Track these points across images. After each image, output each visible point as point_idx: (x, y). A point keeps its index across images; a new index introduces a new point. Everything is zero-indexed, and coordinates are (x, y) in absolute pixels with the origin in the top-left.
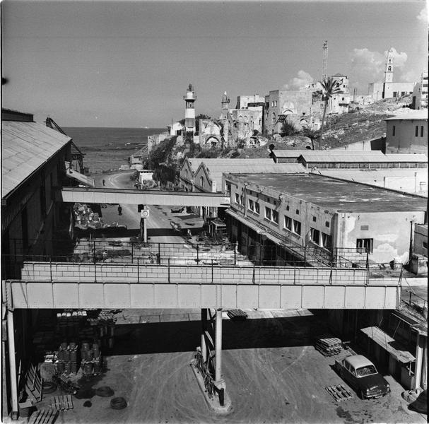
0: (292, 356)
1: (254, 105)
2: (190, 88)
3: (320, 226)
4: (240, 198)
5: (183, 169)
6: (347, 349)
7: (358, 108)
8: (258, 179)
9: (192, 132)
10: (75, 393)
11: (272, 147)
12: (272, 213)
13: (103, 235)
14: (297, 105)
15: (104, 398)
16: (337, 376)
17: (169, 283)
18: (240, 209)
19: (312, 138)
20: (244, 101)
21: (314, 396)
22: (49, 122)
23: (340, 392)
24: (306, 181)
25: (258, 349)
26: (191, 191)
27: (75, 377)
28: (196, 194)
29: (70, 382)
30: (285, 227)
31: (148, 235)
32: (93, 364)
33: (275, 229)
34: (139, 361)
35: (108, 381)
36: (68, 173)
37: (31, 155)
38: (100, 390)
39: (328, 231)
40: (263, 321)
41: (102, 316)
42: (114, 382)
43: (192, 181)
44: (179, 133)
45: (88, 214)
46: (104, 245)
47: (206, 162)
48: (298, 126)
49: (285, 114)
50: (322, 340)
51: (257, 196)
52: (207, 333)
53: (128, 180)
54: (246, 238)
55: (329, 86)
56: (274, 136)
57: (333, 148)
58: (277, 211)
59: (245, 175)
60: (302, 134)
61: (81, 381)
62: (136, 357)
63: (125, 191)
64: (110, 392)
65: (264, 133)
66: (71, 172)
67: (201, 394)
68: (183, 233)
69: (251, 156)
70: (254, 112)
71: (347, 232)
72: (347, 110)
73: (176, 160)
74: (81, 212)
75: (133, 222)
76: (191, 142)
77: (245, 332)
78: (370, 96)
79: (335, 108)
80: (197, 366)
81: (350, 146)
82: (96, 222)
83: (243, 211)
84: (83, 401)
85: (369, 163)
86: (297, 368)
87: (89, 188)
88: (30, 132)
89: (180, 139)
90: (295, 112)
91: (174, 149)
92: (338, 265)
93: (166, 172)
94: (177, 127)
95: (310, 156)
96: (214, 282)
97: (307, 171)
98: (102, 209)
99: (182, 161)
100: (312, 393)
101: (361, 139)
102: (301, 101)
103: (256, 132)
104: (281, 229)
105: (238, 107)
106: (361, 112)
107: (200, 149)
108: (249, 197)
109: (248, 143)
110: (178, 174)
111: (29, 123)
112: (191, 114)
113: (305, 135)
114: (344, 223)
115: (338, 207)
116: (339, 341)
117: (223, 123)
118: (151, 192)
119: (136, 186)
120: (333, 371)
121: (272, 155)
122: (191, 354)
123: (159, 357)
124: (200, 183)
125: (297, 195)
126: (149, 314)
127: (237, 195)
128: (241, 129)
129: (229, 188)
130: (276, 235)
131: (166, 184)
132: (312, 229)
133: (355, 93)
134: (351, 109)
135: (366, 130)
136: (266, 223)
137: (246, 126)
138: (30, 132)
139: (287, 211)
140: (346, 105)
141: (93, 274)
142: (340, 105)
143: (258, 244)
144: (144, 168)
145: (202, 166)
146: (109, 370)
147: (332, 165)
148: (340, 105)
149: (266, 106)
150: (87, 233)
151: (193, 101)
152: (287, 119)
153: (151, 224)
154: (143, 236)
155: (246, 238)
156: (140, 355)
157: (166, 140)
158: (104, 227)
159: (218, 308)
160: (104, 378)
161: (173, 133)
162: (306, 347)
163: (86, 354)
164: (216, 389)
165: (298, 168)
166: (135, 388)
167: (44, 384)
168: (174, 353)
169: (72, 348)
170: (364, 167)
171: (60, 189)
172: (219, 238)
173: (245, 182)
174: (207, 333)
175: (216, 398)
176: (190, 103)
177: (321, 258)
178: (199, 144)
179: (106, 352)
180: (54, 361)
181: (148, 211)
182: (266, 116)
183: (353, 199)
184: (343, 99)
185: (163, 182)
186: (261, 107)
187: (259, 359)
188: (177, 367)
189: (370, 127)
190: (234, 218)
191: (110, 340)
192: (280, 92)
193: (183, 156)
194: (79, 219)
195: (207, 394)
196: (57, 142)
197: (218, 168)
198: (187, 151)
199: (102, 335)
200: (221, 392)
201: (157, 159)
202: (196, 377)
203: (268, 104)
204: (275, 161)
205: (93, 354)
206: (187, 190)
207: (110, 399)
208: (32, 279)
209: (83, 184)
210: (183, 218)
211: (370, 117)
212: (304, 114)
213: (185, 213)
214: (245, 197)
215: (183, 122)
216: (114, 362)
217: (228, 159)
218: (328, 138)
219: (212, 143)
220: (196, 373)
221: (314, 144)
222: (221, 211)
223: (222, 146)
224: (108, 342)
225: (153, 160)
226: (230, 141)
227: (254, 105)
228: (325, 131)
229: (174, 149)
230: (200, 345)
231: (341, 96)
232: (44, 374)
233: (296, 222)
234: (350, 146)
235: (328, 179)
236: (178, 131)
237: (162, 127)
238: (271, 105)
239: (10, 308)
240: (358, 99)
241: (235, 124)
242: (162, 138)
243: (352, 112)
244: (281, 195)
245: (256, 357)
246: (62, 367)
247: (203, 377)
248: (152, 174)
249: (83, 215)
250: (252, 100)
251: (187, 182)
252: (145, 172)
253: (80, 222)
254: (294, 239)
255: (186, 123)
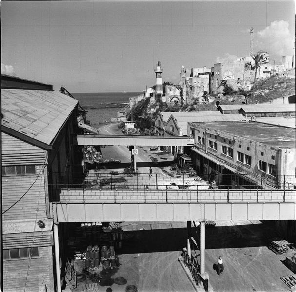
0: (252, 254)
1: (203, 74)
2: (159, 64)
3: (267, 159)
4: (201, 139)
5: (157, 120)
6: (292, 248)
7: (277, 74)
8: (214, 126)
9: (161, 94)
10: (99, 282)
11: (218, 103)
12: (227, 150)
13: (104, 167)
14: (235, 73)
15: (121, 285)
16: (288, 269)
17: (167, 203)
18: (201, 148)
19: (245, 95)
20: (196, 72)
21: (273, 284)
22: (63, 90)
23: (293, 281)
24: (248, 126)
25: (226, 249)
26: (163, 135)
27: (98, 270)
28: (167, 137)
29: (95, 274)
30: (238, 160)
31: (137, 167)
32: (110, 260)
33: (230, 161)
34: (174, 253)
35: (121, 273)
36: (79, 124)
37: (58, 113)
38: (117, 279)
39: (273, 162)
40: (227, 228)
41: (83, 225)
42: (126, 273)
43: (164, 128)
44: (151, 95)
45: (93, 153)
46: (106, 174)
47: (175, 114)
48: (235, 88)
49: (226, 79)
50: (275, 242)
51: (216, 138)
52: (192, 238)
53: (117, 128)
54: (207, 167)
55: (257, 59)
56: (219, 95)
57: (261, 102)
58: (232, 148)
59: (204, 123)
60: (239, 93)
61: (103, 273)
62: (139, 254)
63: (121, 136)
64: (124, 281)
65: (211, 92)
66: (81, 124)
67: (190, 283)
68: (162, 165)
69: (203, 110)
70: (204, 79)
71: (288, 163)
72: (269, 75)
73: (150, 114)
74: (89, 151)
75: (124, 158)
76: (160, 101)
77: (223, 237)
78: (283, 66)
79: (262, 76)
80: (185, 262)
81: (274, 101)
82: (100, 158)
83: (204, 149)
84: (106, 287)
85: (290, 112)
86: (258, 263)
87: (94, 135)
88: (52, 97)
89: (153, 99)
90: (233, 78)
91: (149, 106)
92: (282, 188)
93: (144, 123)
94: (150, 91)
95: (247, 108)
96: (199, 202)
97: (248, 119)
98: (101, 149)
99: (154, 114)
100: (271, 282)
101: (281, 95)
102: (237, 70)
103: (205, 93)
104: (235, 162)
105: (192, 75)
106: (280, 77)
107: (166, 106)
108: (209, 139)
109: (200, 100)
110: (153, 123)
111: (50, 91)
112: (159, 81)
113: (240, 94)
114: (286, 156)
115: (278, 145)
116: (287, 243)
117: (182, 87)
118: (133, 137)
119: (124, 132)
120: (284, 265)
121: (219, 109)
122: (178, 253)
123: (156, 254)
124: (170, 129)
125: (246, 136)
126: (145, 224)
127: (200, 138)
128: (196, 91)
129: (193, 134)
130: (231, 166)
131: (144, 131)
132: (260, 161)
133: (274, 64)
134: (272, 75)
135: (284, 89)
136: (222, 157)
137: (199, 89)
138: (52, 97)
139: (240, 149)
140: (268, 72)
141: (113, 197)
142: (264, 72)
143: (217, 172)
144: (128, 120)
145: (172, 118)
146: (121, 264)
147: (263, 114)
148: (264, 72)
149: (212, 75)
150: (94, 166)
151: (160, 73)
152: (227, 83)
153: (138, 159)
154: (133, 168)
155: (207, 167)
156: (142, 254)
157: (142, 100)
158: (105, 161)
159: (202, 221)
160: (118, 271)
161: (147, 95)
162: (261, 247)
163: (105, 253)
164: (202, 279)
165: (239, 117)
166: (141, 278)
167: (77, 275)
168: (166, 252)
169: (96, 249)
170: (287, 115)
171: (76, 136)
172: (187, 169)
173: (206, 128)
174: (192, 238)
175: (201, 286)
176: (159, 74)
177: (268, 182)
178: (165, 102)
179: (119, 251)
180: (82, 258)
181: (137, 150)
182: (212, 81)
183: (287, 139)
184: (266, 68)
185: (142, 130)
186: (208, 75)
187: (228, 256)
188: (170, 262)
189: (287, 87)
190: (198, 154)
191: (120, 242)
192: (221, 65)
193: (155, 111)
194: (87, 156)
195: (194, 283)
196: (72, 104)
197: (183, 120)
198: (158, 107)
199: (114, 239)
200: (205, 283)
201: (137, 113)
202: (184, 269)
203: (213, 73)
204: (222, 113)
205: (110, 253)
206: (160, 134)
207: (125, 286)
208: (71, 201)
209: (90, 132)
210: (159, 154)
211: (286, 80)
212: (239, 79)
213: (159, 151)
214: (206, 138)
215: (154, 88)
216: (125, 258)
217: (187, 112)
218: (257, 96)
219: (175, 101)
220: (184, 267)
221: (248, 100)
222: (187, 149)
223: (182, 103)
224: (118, 244)
225: (134, 114)
226: (188, 100)
227: (203, 74)
228: (255, 91)
229: (149, 106)
230: (186, 247)
231: (265, 65)
232: (76, 268)
233: (247, 156)
234: (274, 101)
235: (264, 125)
236: (151, 94)
237: (140, 92)
238: (215, 73)
239: (55, 222)
240: (276, 68)
241: (191, 88)
242: (139, 99)
243: (273, 77)
244: (235, 137)
245: (225, 256)
246: (89, 263)
247: (190, 269)
248: (134, 124)
249: (90, 153)
250: (201, 71)
251: (160, 129)
252: (129, 123)
253: (88, 158)
254: (245, 168)
255: (156, 88)
